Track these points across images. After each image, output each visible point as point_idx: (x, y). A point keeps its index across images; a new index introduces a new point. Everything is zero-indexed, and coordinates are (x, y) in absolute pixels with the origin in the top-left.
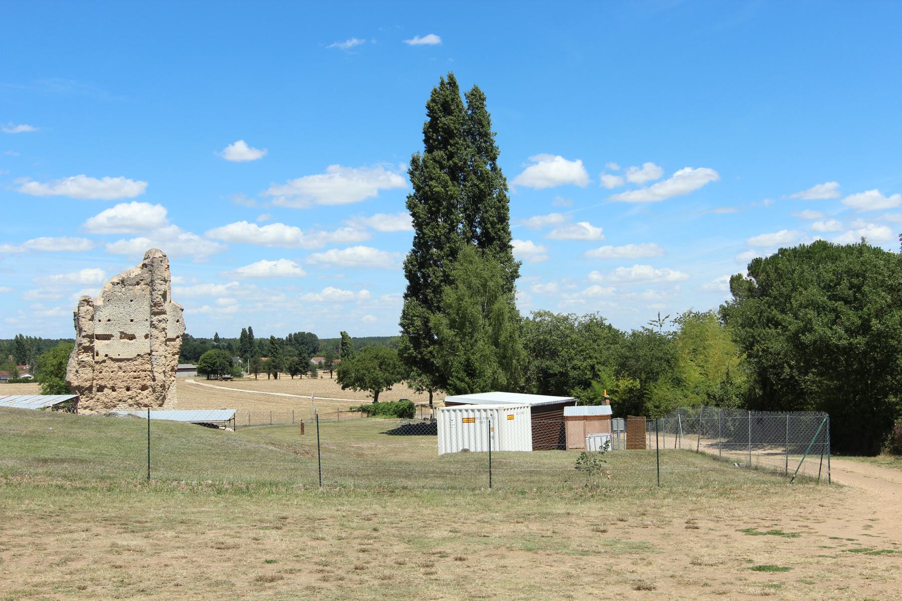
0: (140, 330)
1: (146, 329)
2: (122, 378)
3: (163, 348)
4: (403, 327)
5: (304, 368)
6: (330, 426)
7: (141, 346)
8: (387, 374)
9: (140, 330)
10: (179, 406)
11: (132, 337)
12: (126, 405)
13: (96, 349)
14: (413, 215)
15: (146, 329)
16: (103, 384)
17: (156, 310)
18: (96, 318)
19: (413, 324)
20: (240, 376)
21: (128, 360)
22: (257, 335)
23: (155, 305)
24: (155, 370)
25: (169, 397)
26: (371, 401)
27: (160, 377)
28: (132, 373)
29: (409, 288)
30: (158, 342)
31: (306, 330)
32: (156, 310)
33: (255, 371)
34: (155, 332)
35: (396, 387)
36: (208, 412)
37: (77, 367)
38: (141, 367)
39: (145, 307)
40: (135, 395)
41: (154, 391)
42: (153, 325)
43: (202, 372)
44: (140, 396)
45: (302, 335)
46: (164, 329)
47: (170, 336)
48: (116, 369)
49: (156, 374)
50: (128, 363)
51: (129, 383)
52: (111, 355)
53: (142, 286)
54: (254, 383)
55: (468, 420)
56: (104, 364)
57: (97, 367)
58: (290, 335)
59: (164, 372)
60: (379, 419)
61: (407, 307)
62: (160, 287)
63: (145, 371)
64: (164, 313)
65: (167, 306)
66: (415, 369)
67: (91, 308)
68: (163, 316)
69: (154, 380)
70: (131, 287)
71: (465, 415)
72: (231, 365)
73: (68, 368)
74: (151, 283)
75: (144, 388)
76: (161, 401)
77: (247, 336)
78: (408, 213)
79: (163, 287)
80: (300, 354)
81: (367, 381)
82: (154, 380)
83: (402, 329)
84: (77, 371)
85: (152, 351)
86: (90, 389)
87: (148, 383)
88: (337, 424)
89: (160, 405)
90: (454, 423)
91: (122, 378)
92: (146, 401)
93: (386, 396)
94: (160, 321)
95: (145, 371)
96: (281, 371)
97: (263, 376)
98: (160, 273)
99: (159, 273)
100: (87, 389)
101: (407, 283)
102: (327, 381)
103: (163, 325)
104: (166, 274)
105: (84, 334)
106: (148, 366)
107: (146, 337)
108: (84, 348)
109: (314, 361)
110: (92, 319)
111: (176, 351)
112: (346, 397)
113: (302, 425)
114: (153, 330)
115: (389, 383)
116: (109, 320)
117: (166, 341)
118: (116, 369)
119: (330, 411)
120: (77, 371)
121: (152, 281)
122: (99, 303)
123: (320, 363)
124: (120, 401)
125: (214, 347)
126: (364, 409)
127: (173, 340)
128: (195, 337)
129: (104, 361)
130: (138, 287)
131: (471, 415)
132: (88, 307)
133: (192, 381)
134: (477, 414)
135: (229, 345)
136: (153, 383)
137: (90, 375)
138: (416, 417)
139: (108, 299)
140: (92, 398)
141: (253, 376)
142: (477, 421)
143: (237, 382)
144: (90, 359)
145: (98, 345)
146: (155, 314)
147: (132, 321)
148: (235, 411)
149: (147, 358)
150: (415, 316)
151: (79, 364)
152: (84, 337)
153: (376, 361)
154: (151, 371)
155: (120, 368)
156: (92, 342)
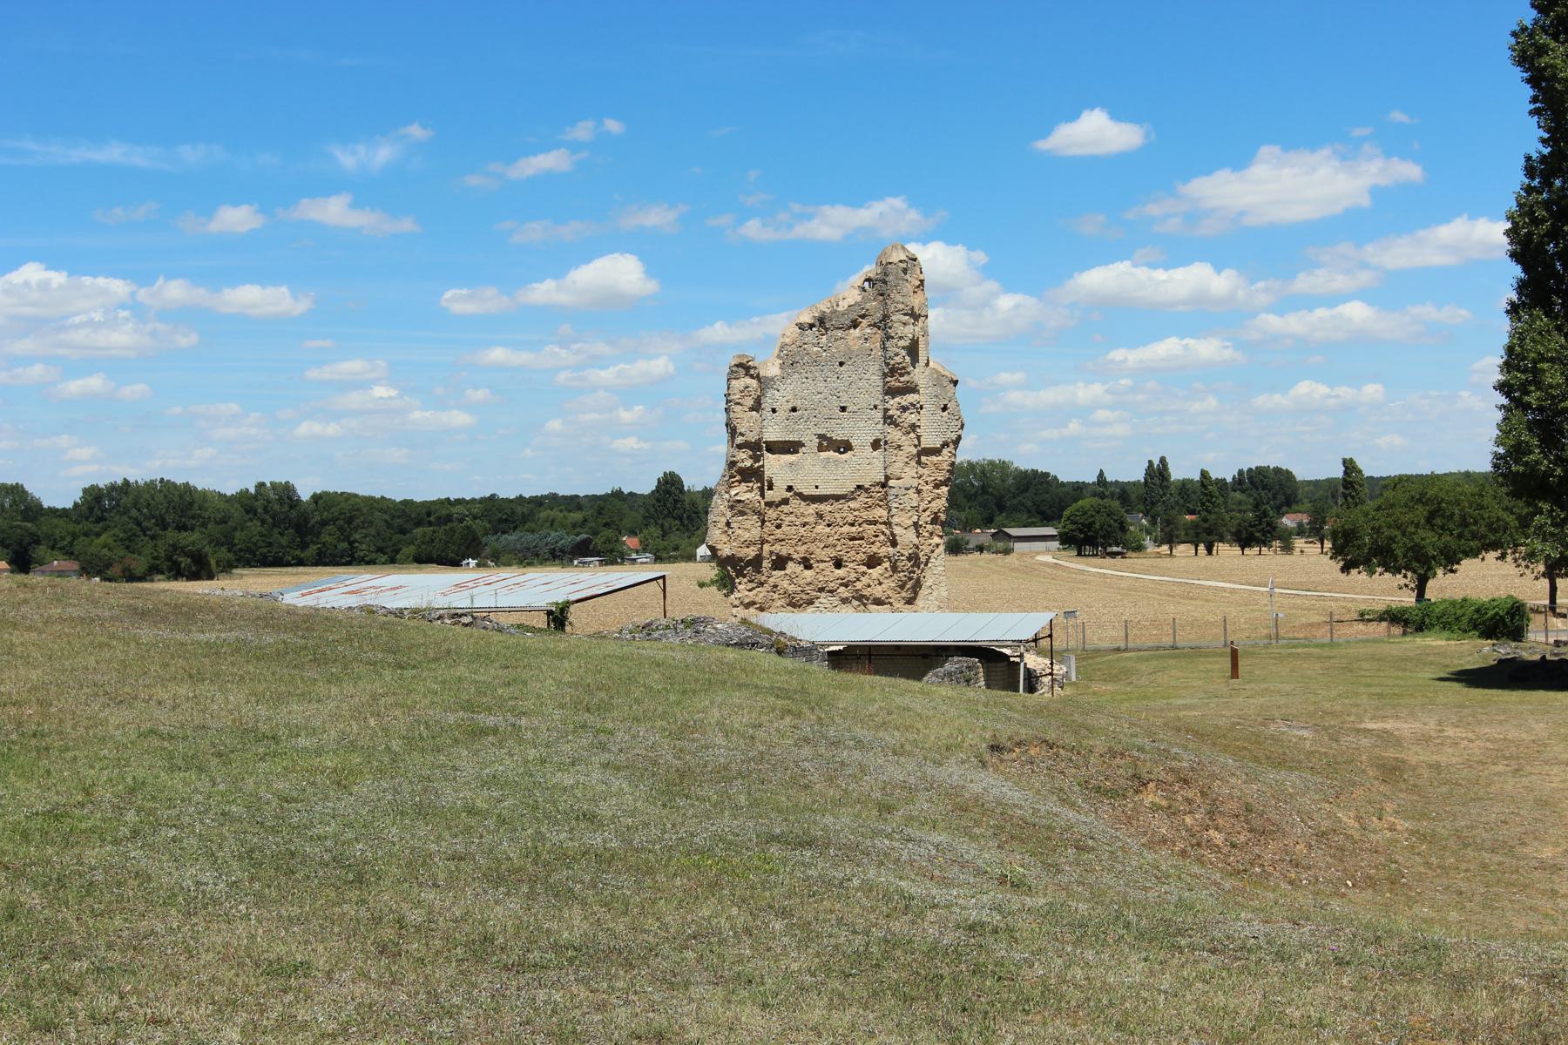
0: (861, 431)
1: (875, 429)
2: (824, 538)
4: (1508, 395)
5: (1264, 533)
6: (1307, 657)
7: (864, 466)
8: (1446, 538)
9: (861, 431)
10: (949, 605)
11: (845, 447)
12: (835, 600)
13: (767, 474)
14: (1533, 81)
15: (875, 429)
16: (784, 552)
17: (896, 383)
18: (767, 403)
19: (1538, 384)
20: (1139, 548)
21: (837, 498)
22: (1177, 473)
23: (893, 371)
24: (895, 520)
25: (928, 582)
26: (1408, 599)
27: (907, 537)
28: (846, 529)
29: (1522, 287)
30: (902, 457)
31: (1271, 460)
32: (896, 383)
33: (1170, 539)
34: (894, 435)
35: (1467, 566)
36: (461, 601)
37: (729, 514)
38: (865, 515)
39: (872, 379)
40: (853, 576)
41: (894, 569)
42: (889, 420)
43: (1067, 540)
44: (865, 580)
45: (1261, 471)
46: (914, 427)
47: (927, 442)
48: (811, 519)
49: (897, 530)
50: (837, 505)
53: (864, 329)
54: (1166, 562)
56: (785, 508)
57: (771, 513)
58: (1241, 472)
59: (916, 525)
60: (1434, 642)
61: (1519, 336)
62: (904, 330)
63: (875, 523)
64: (912, 389)
65: (919, 375)
66: (1546, 507)
67: (754, 383)
68: (911, 398)
69: (894, 544)
70: (839, 333)
72: (1123, 528)
73: (711, 517)
74: (883, 324)
75: (872, 562)
76: (911, 592)
77: (1158, 473)
78: (1518, 74)
79: (908, 331)
80: (1257, 506)
81: (1399, 553)
82: (894, 544)
83: (1504, 401)
84: (728, 524)
85: (887, 478)
86: (756, 562)
88: (1326, 652)
89: (910, 601)
91: (824, 538)
92: (878, 592)
93: (1442, 587)
94: (904, 409)
95: (875, 523)
96: (1221, 540)
97: (1183, 549)
98: (905, 296)
99: (898, 298)
100: (749, 563)
101: (1517, 271)
102: (1312, 560)
103: (911, 418)
104: (916, 301)
105: (739, 440)
106: (880, 513)
107: (876, 445)
108: (742, 471)
109: (1288, 521)
110: (757, 407)
112: (1353, 590)
113: (1234, 654)
114: (890, 429)
115: (1450, 560)
116: (794, 410)
117: (919, 454)
118: (811, 519)
119: (1316, 619)
120: (728, 524)
121: (885, 317)
122: (772, 370)
123: (1300, 525)
124: (821, 590)
125: (1094, 495)
126: (1393, 617)
127: (936, 451)
128: (1063, 478)
129: (785, 502)
130: (856, 333)
132: (748, 381)
133: (1048, 559)
135: (1123, 492)
137: (756, 533)
138: (1531, 636)
139: (791, 361)
140: (761, 584)
141: (1165, 548)
143: (1134, 560)
145: (773, 465)
146: (892, 392)
147: (843, 409)
148: (1051, 615)
150: (1543, 359)
151: (732, 507)
152: (740, 447)
153: (1420, 508)
154: (888, 524)
155: (820, 516)
156: (757, 458)
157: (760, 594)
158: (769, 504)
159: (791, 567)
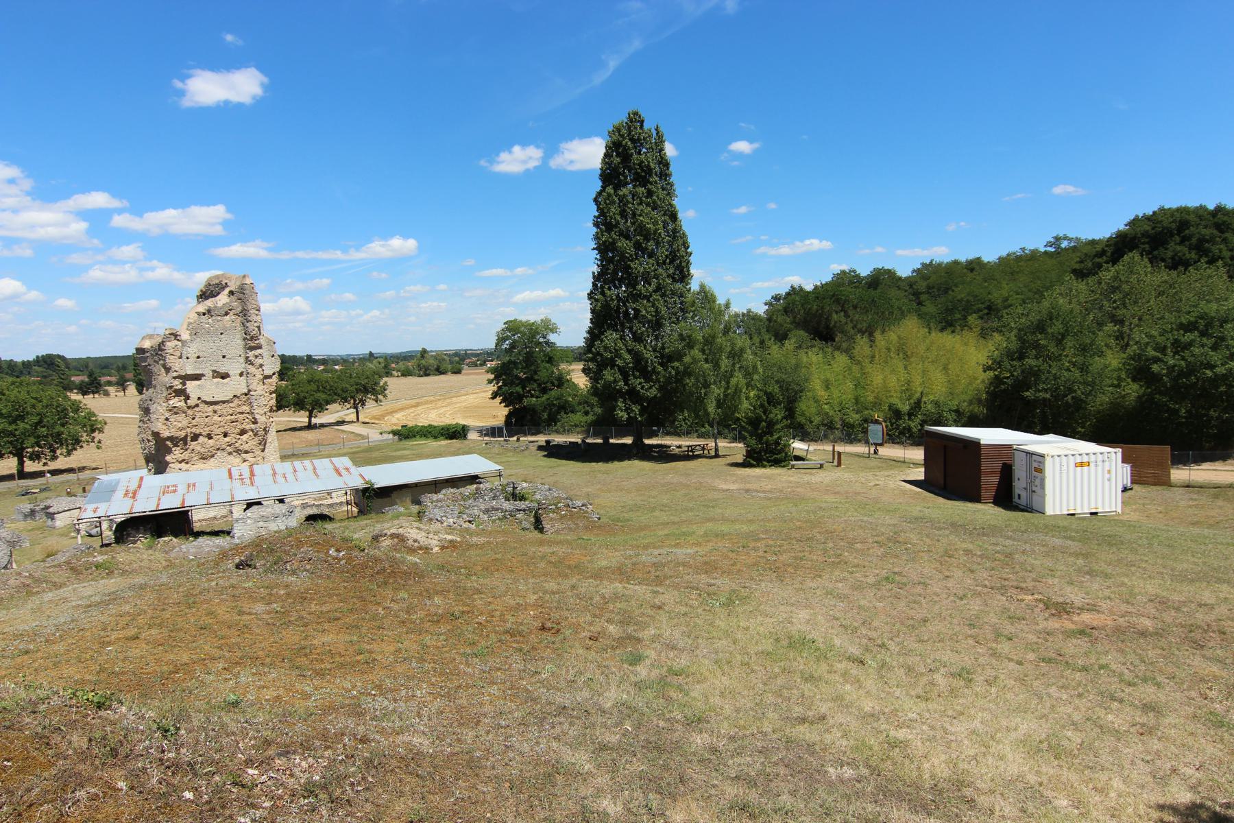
2: (217, 422)
3: (260, 387)
7: (236, 385)
11: (224, 376)
13: (188, 391)
21: (224, 402)
23: (252, 338)
27: (262, 419)
30: (256, 380)
34: (252, 369)
38: (238, 410)
42: (247, 360)
46: (261, 365)
49: (257, 416)
51: (227, 429)
52: (204, 398)
55: (1082, 465)
57: (190, 412)
64: (259, 347)
65: (262, 341)
68: (258, 352)
69: (255, 422)
71: (1079, 460)
75: (243, 432)
82: (255, 422)
86: (184, 439)
87: (248, 427)
90: (1065, 468)
92: (246, 447)
103: (260, 361)
106: (246, 408)
107: (241, 374)
111: (273, 389)
129: (197, 406)
130: (227, 318)
131: (1085, 459)
134: (1093, 458)
136: (253, 426)
137: (185, 423)
142: (1092, 465)
144: (182, 404)
145: (191, 386)
146: (252, 349)
149: (244, 398)
155: (215, 412)
156: (184, 384)
157: (186, 455)
158: (189, 408)
159: (201, 439)
